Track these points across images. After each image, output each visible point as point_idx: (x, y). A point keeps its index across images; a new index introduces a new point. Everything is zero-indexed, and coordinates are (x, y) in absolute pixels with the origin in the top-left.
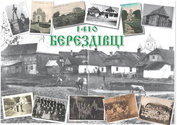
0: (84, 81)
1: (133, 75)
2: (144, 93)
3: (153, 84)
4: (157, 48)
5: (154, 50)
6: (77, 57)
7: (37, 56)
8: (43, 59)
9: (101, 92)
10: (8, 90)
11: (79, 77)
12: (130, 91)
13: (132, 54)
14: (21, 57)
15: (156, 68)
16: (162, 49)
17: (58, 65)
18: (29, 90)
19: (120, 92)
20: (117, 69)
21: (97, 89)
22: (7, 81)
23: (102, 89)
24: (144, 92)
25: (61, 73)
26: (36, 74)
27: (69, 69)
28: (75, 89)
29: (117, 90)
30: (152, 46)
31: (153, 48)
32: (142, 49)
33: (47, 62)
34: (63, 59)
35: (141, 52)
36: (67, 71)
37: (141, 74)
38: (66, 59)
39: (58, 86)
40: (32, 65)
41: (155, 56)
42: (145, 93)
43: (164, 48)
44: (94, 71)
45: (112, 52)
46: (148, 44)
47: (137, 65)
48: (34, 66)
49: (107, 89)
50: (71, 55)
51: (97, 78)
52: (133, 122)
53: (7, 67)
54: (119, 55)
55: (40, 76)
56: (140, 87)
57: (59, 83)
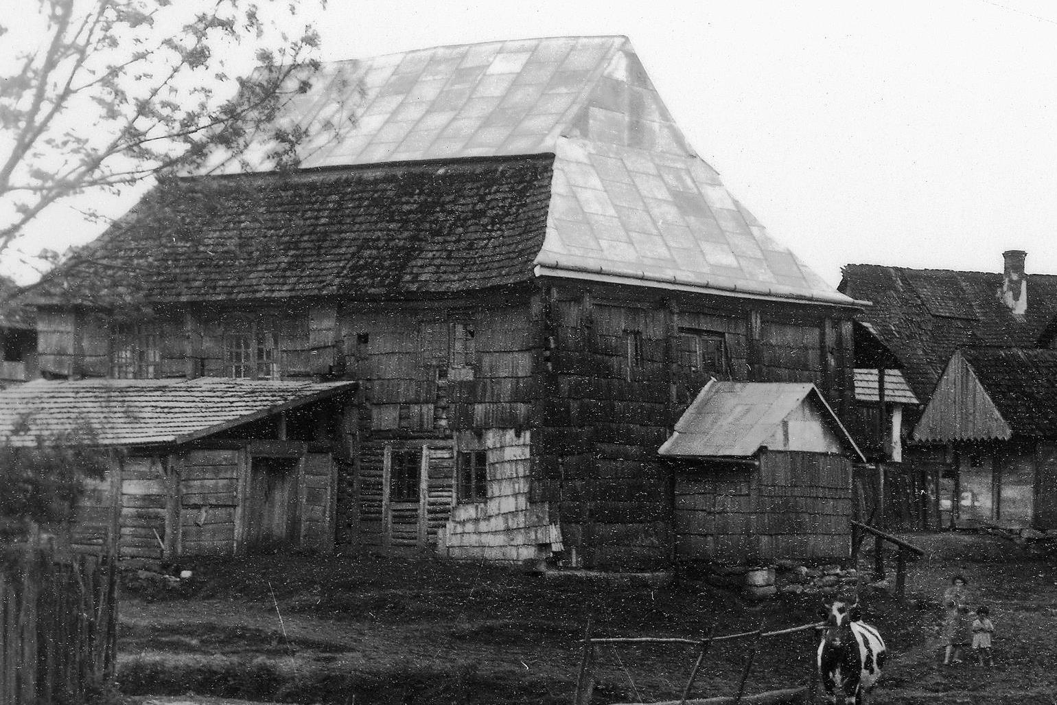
26: (531, 562)
34: (897, 365)
40: (479, 435)
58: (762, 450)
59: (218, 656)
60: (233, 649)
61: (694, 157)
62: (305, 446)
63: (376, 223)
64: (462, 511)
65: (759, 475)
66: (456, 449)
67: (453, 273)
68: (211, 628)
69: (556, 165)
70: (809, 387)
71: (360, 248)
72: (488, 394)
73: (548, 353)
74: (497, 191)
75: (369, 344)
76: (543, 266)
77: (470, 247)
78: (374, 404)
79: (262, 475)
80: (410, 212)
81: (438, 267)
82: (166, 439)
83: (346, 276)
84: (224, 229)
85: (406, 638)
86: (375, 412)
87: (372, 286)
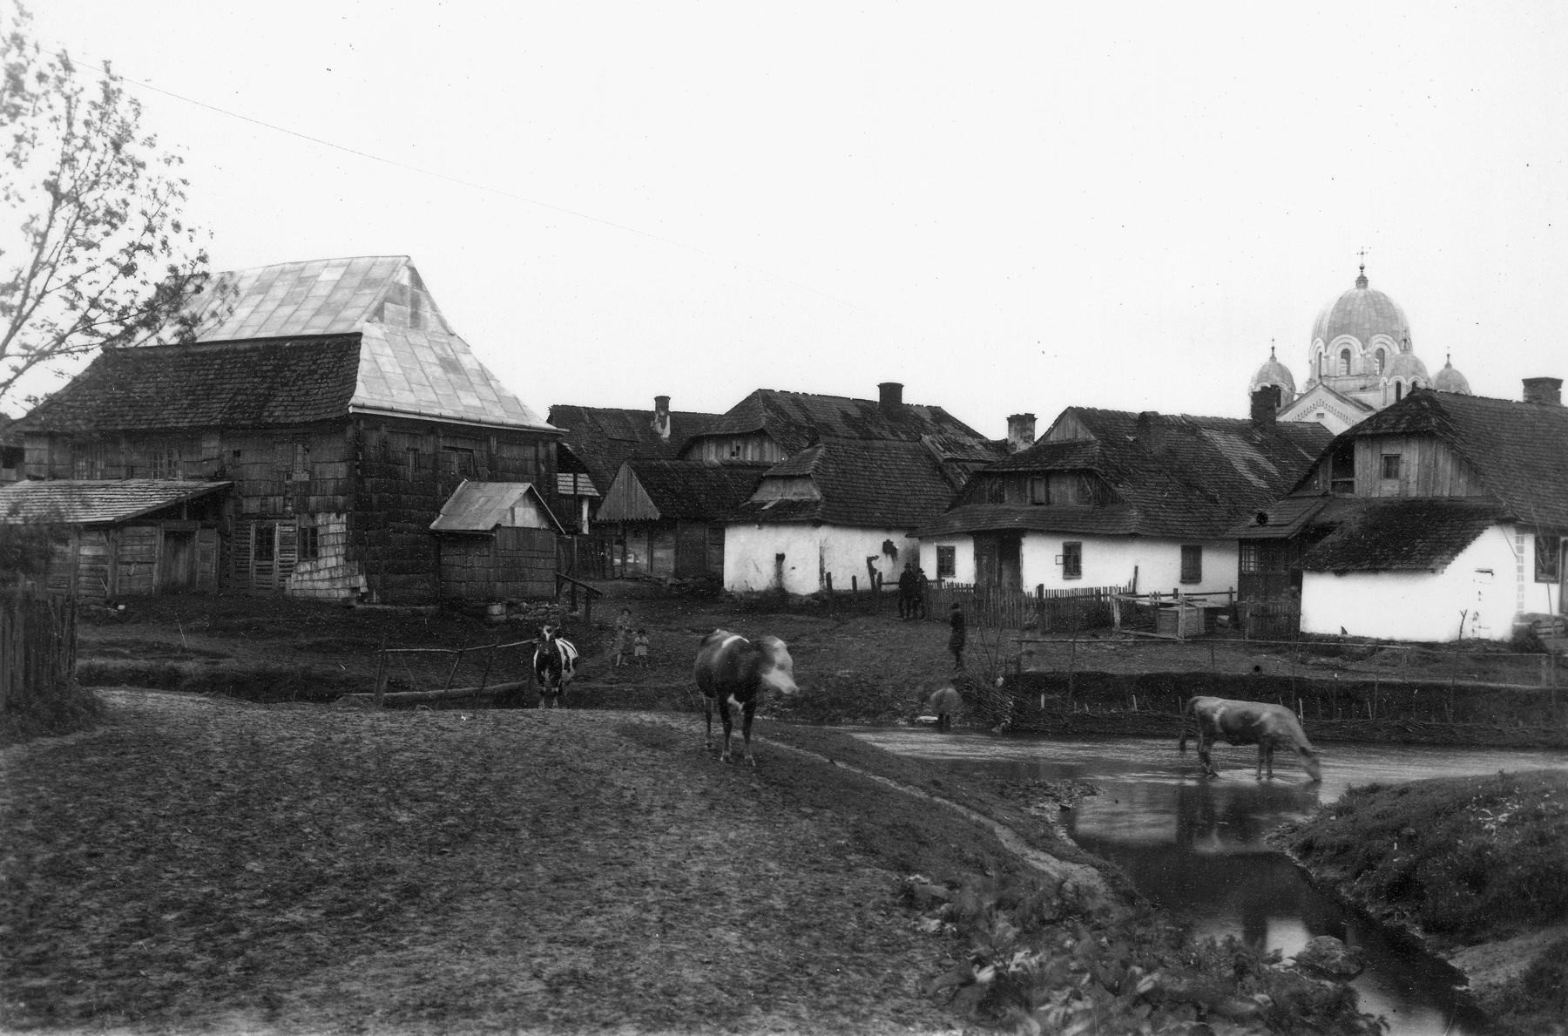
0: (771, 662)
1: (1212, 613)
2: (1303, 761)
3: (1383, 685)
4: (1422, 385)
5: (1392, 400)
6: (713, 456)
7: (359, 444)
8: (409, 471)
9: (931, 748)
10: (100, 731)
11: (725, 627)
12: (1183, 748)
13: (1206, 433)
14: (212, 447)
15: (1407, 557)
16: (1466, 396)
18: (285, 733)
19: (1091, 754)
20: (1072, 565)
21: (896, 728)
22: (92, 655)
23: (941, 731)
24: (1304, 751)
25: (567, 587)
26: (347, 599)
27: (643, 560)
28: (689, 726)
29: (1063, 734)
30: (1382, 366)
31: (1388, 381)
32: (1293, 389)
33: (447, 494)
34: (586, 472)
35: (1281, 419)
36: (622, 577)
37: (1280, 604)
38: (617, 469)
39: (535, 705)
40: (313, 516)
41: (1405, 456)
42: (1316, 763)
43: (1480, 386)
44: (872, 571)
45: (1029, 419)
46: (1346, 354)
47: (1247, 526)
48: (334, 527)
49: (979, 731)
50: (655, 436)
51: (895, 631)
52: (1199, 1008)
53: (94, 537)
54: (1087, 443)
55: (379, 612)
56: (1268, 713)
57: (546, 674)
62: (199, 524)
67: (296, 411)
68: (138, 643)
71: (235, 394)
77: (307, 394)
79: (171, 543)
80: (269, 371)
83: (226, 413)
84: (147, 382)
86: (245, 502)
87: (243, 419)
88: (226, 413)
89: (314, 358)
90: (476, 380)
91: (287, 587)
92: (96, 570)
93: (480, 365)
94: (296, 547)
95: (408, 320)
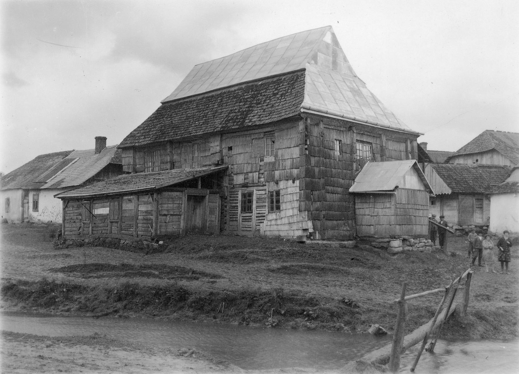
17: (422, 188)
26: (301, 237)
31: (460, 200)
34: (430, 161)
40: (277, 183)
53: (145, 199)
58: (397, 187)
59: (166, 280)
60: (172, 277)
61: (355, 77)
62: (208, 191)
63: (235, 104)
64: (270, 216)
65: (396, 199)
66: (267, 190)
67: (266, 117)
68: (165, 266)
69: (306, 72)
70: (414, 161)
71: (230, 113)
72: (281, 166)
73: (306, 146)
74: (283, 85)
75: (233, 151)
76: (304, 108)
77: (272, 106)
78: (234, 174)
79: (192, 203)
80: (248, 98)
81: (260, 115)
82: (152, 187)
83: (223, 124)
84: (182, 115)
85: (248, 271)
86: (235, 177)
87: (233, 125)
88: (223, 124)
89: (276, 87)
90: (370, 100)
91: (261, 229)
92: (147, 220)
93: (372, 94)
94: (267, 204)
95: (331, 66)
